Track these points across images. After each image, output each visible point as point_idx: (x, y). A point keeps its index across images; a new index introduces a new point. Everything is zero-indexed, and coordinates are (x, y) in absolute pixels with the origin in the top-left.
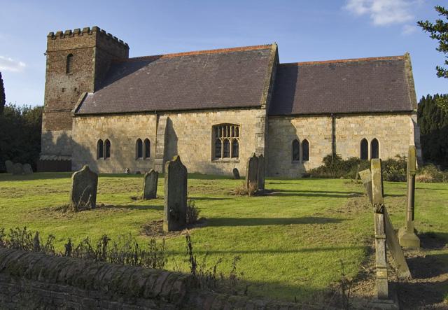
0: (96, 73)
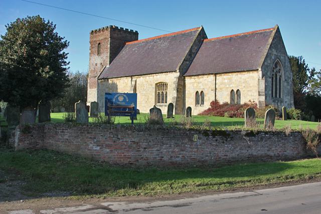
0: (110, 53)
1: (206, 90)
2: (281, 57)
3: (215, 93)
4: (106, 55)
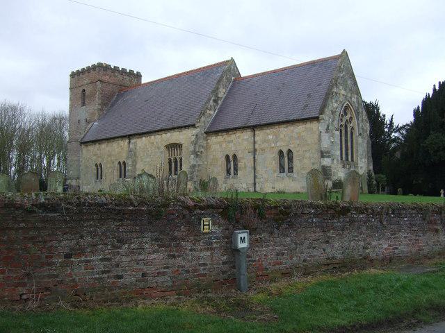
1: (240, 152)
2: (353, 99)
4: (94, 106)
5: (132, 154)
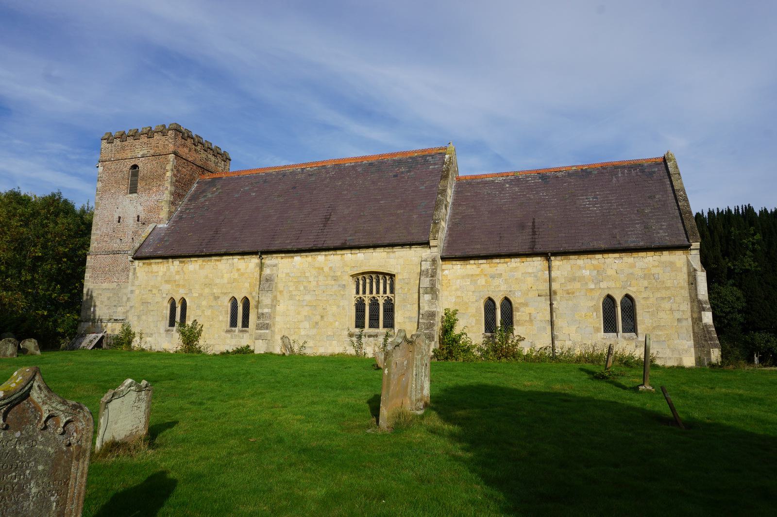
1: (518, 294)
3: (551, 304)
5: (266, 283)
